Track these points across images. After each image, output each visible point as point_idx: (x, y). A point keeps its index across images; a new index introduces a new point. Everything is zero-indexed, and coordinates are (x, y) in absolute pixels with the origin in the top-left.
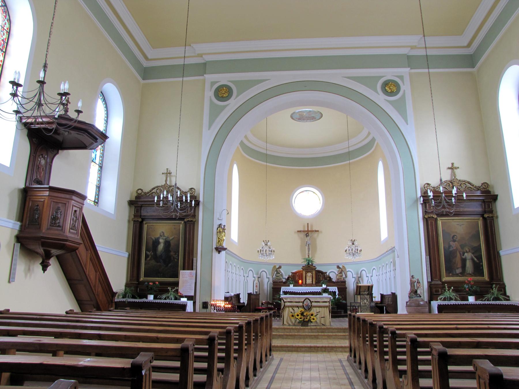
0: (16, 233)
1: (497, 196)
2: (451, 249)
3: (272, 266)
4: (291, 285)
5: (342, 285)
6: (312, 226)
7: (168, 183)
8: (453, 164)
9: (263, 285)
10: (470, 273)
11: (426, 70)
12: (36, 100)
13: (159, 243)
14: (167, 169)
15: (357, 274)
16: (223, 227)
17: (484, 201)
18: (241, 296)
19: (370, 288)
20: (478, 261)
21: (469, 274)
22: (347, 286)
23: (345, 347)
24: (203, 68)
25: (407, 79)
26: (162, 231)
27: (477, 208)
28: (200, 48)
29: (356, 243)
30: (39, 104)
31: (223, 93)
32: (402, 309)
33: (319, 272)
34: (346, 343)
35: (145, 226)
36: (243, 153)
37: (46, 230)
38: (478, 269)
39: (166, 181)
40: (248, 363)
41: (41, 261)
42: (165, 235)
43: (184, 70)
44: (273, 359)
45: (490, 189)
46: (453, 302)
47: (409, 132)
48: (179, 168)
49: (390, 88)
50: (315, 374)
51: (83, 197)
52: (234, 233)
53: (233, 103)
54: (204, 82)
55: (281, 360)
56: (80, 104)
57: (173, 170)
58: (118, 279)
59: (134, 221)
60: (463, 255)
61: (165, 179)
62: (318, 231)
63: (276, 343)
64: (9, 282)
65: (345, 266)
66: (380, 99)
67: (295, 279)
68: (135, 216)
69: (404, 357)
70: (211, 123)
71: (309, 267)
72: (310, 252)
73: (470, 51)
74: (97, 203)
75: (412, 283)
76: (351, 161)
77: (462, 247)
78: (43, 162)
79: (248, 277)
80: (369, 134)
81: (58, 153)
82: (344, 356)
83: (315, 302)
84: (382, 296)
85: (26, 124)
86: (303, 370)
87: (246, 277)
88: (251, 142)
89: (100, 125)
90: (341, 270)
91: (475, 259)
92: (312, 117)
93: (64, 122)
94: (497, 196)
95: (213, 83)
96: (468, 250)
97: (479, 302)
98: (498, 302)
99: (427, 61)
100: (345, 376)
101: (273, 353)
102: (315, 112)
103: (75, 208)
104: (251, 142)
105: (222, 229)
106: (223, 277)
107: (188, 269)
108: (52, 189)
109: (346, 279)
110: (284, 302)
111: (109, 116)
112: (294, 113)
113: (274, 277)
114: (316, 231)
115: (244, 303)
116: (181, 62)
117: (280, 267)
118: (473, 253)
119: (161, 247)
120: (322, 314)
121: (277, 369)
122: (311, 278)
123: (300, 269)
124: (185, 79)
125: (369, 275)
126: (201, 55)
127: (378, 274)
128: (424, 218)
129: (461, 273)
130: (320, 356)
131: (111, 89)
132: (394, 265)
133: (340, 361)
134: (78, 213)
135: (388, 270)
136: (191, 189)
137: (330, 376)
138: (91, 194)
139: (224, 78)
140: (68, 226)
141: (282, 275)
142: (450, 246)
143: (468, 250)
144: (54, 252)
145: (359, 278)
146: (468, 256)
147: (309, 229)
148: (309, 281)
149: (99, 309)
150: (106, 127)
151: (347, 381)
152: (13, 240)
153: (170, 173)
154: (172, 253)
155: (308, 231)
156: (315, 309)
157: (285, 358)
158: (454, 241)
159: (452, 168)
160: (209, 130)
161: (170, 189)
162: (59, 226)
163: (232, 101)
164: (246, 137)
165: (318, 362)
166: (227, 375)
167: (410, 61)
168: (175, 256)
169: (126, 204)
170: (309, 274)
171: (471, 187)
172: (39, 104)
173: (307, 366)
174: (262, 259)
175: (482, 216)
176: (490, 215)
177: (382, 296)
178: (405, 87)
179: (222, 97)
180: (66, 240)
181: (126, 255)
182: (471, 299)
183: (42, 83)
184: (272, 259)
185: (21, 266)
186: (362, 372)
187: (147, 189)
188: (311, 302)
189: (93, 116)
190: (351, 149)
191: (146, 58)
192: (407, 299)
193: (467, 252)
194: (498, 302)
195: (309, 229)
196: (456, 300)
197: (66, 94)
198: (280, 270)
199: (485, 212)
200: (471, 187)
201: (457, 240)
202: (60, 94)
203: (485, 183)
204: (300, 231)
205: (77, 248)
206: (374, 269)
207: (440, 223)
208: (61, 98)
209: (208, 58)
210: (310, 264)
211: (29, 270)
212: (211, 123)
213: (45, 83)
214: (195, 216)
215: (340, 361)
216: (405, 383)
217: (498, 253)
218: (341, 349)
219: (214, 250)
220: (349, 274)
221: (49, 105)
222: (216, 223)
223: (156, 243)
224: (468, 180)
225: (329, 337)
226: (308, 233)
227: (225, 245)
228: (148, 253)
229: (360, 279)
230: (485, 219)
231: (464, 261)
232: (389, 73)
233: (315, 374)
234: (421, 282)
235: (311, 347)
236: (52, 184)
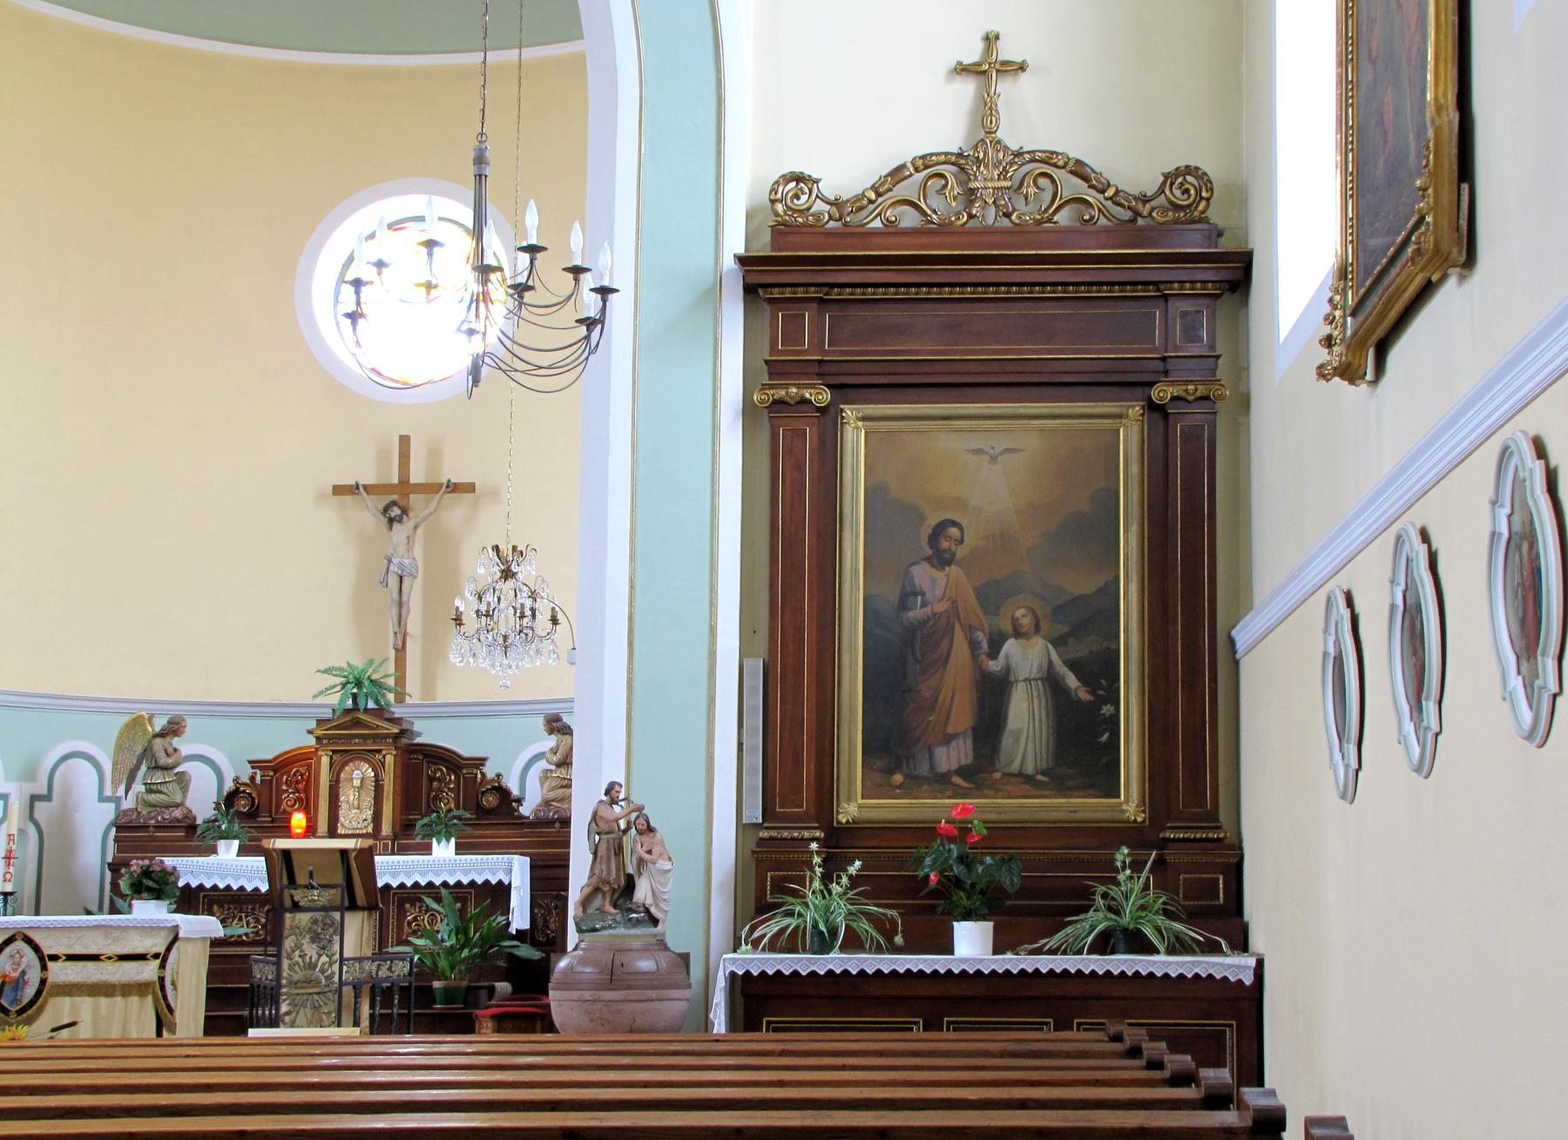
2: (916, 614)
4: (222, 844)
6: (434, 455)
8: (990, 40)
9: (69, 846)
10: (1030, 769)
20: (1084, 695)
21: (1028, 779)
29: (526, 571)
38: (1082, 745)
46: (836, 961)
60: (993, 655)
62: (470, 488)
77: (991, 596)
83: (71, 958)
96: (1026, 622)
97: (1013, 962)
98: (1122, 963)
114: (454, 488)
117: (174, 728)
118: (1058, 642)
122: (368, 800)
123: (296, 737)
129: (962, 772)
142: (908, 595)
143: (1026, 622)
146: (1026, 657)
147: (416, 477)
156: (66, 1002)
158: (941, 560)
159: (988, 69)
170: (360, 773)
171: (1091, 196)
182: (971, 944)
188: (44, 960)
193: (1018, 634)
194: (1122, 963)
195: (416, 477)
196: (853, 943)
198: (176, 742)
200: (1091, 196)
201: (961, 552)
203: (1189, 170)
204: (353, 490)
207: (855, 438)
224: (1074, 154)
231: (993, 692)
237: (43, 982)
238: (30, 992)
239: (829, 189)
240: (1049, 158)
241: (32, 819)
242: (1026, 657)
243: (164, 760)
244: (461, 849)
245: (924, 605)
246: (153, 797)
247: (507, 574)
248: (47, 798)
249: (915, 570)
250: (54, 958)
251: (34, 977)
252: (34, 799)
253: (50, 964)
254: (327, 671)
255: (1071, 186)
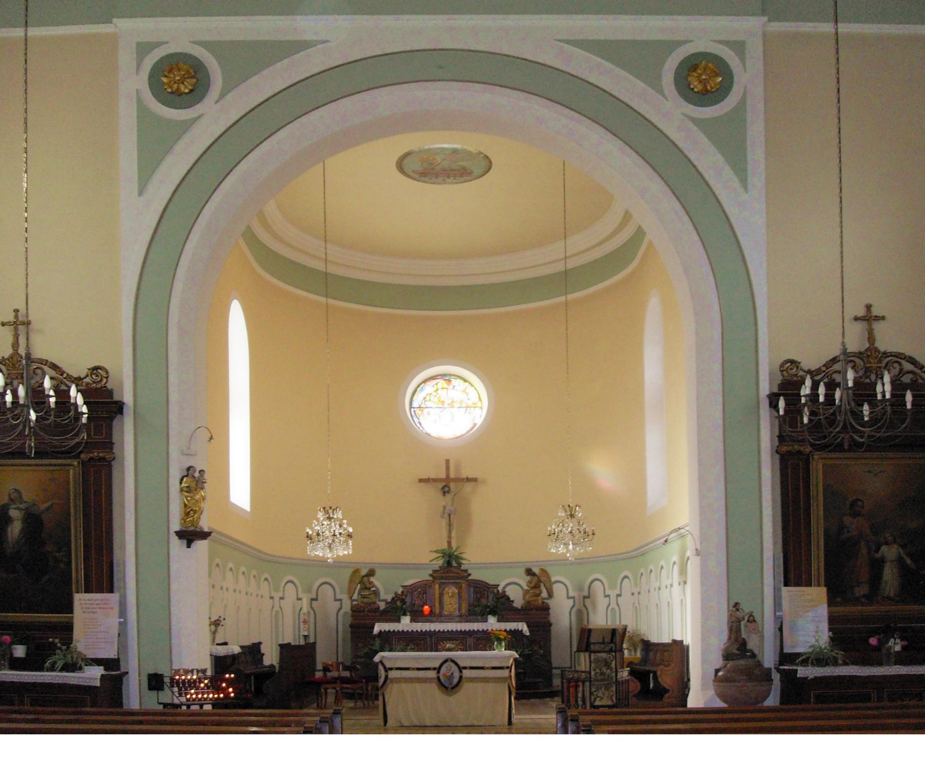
3: (348, 573)
5: (537, 614)
6: (458, 466)
8: (869, 307)
10: (892, 595)
11: (827, 28)
14: (16, 311)
15: (580, 589)
16: (197, 475)
18: (263, 649)
21: (889, 598)
22: (552, 619)
31: (180, 80)
33: (481, 588)
39: (15, 345)
42: (25, 498)
53: (212, 117)
54: (112, 41)
60: (877, 550)
61: (10, 339)
65: (548, 569)
71: (451, 567)
72: (453, 534)
76: (570, 297)
79: (282, 598)
80: (627, 217)
83: (472, 668)
87: (277, 599)
88: (282, 241)
90: (538, 579)
91: (909, 561)
95: (143, 49)
102: (469, 155)
104: (282, 241)
105: (193, 480)
107: (100, 590)
109: (550, 602)
110: (387, 670)
113: (355, 596)
115: (272, 666)
117: (371, 573)
118: (903, 546)
123: (425, 576)
125: (613, 593)
127: (636, 591)
129: (864, 596)
136: (96, 368)
141: (376, 593)
145: (585, 600)
147: (452, 475)
154: (49, 548)
155: (448, 479)
159: (869, 318)
160: (140, 193)
163: (207, 106)
170: (451, 590)
171: (916, 370)
178: (748, 78)
179: (178, 93)
188: (461, 669)
190: (571, 264)
193: (887, 544)
195: (452, 475)
198: (372, 579)
200: (916, 370)
206: (626, 577)
210: (454, 564)
219: (175, 541)
220: (558, 590)
226: (450, 484)
227: (205, 524)
229: (587, 601)
231: (877, 566)
234: (758, 619)
237: (461, 677)
238: (455, 681)
240: (899, 356)
241: (312, 608)
242: (890, 552)
243: (368, 586)
244: (499, 621)
245: (848, 532)
246: (365, 600)
247: (572, 516)
248: (316, 599)
249: (845, 519)
250: (465, 668)
251: (457, 675)
252: (312, 600)
253: (464, 671)
254: (437, 552)
255: (908, 366)
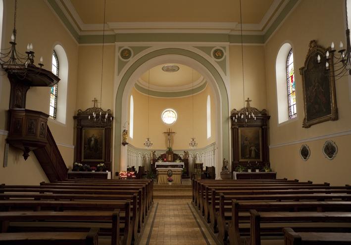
0: (6, 137)
1: (270, 116)
5: (186, 161)
7: (96, 106)
8: (248, 98)
12: (10, 55)
13: (91, 140)
17: (263, 119)
18: (135, 167)
19: (201, 165)
23: (190, 196)
24: (114, 38)
25: (227, 49)
26: (94, 133)
27: (259, 123)
28: (112, 25)
29: (195, 140)
30: (13, 58)
31: (126, 54)
32: (218, 177)
34: (191, 194)
35: (84, 131)
36: (141, 93)
37: (27, 134)
38: (257, 156)
39: (94, 105)
40: (143, 210)
41: (23, 154)
43: (103, 39)
44: (154, 204)
45: (267, 113)
47: (227, 80)
48: (101, 96)
49: (218, 54)
50: (176, 213)
51: (48, 116)
52: (131, 134)
53: (132, 61)
54: (115, 46)
55: (158, 204)
56: (41, 60)
57: (98, 99)
58: (69, 160)
59: (77, 128)
63: (155, 193)
64: (4, 167)
66: (212, 60)
67: (163, 157)
68: (77, 125)
69: (218, 201)
70: (119, 72)
71: (170, 151)
73: (263, 33)
74: (55, 118)
75: (224, 162)
76: (194, 94)
78: (20, 94)
81: (29, 88)
82: (190, 201)
84: (207, 167)
85: (6, 70)
86: (170, 210)
89: (54, 71)
90: (186, 153)
92: (174, 69)
93: (30, 69)
94: (270, 116)
95: (120, 48)
99: (242, 39)
100: (191, 214)
101: (154, 200)
103: (42, 122)
105: (126, 132)
106: (127, 160)
108: (27, 111)
111: (59, 65)
112: (164, 67)
116: (102, 33)
117: (155, 152)
119: (93, 142)
120: (177, 178)
121: (156, 209)
123: (164, 153)
124: (105, 44)
126: (112, 30)
128: (232, 128)
130: (177, 201)
131: (59, 48)
132: (214, 152)
133: (188, 204)
134: (44, 125)
135: (208, 155)
137: (184, 213)
138: (51, 113)
139: (126, 45)
140: (38, 133)
142: (244, 143)
144: (31, 148)
145: (195, 158)
146: (253, 148)
148: (170, 159)
149: (59, 180)
150: (58, 72)
151: (193, 217)
152: (4, 142)
153: (97, 101)
154: (99, 146)
157: (160, 203)
158: (247, 140)
159: (248, 101)
161: (96, 110)
162: (33, 133)
164: (138, 81)
165: (176, 205)
166: (135, 220)
167: (230, 38)
168: (101, 148)
169: (72, 118)
170: (170, 156)
172: (13, 58)
173: (171, 207)
174: (147, 148)
175: (261, 127)
176: (266, 127)
177: (207, 167)
178: (226, 54)
180: (38, 142)
181: (73, 147)
183: (14, 44)
184: (151, 148)
185: (11, 158)
186: (201, 214)
187: (84, 109)
189: (50, 64)
190: (194, 88)
191: (80, 30)
192: (221, 171)
197: (32, 53)
199: (263, 125)
202: (27, 53)
205: (45, 146)
207: (240, 131)
208: (29, 55)
209: (117, 32)
211: (16, 159)
212: (119, 72)
213: (16, 44)
214: (111, 125)
215: (188, 204)
216: (231, 226)
217: (268, 147)
218: (188, 197)
219: (122, 144)
220: (190, 155)
221: (21, 60)
222: (123, 129)
223: (90, 140)
225: (181, 190)
226: (169, 133)
228: (86, 146)
230: (263, 129)
231: (250, 151)
232: (218, 45)
233: (176, 213)
235: (172, 196)
236: (27, 108)
239: (237, 110)
